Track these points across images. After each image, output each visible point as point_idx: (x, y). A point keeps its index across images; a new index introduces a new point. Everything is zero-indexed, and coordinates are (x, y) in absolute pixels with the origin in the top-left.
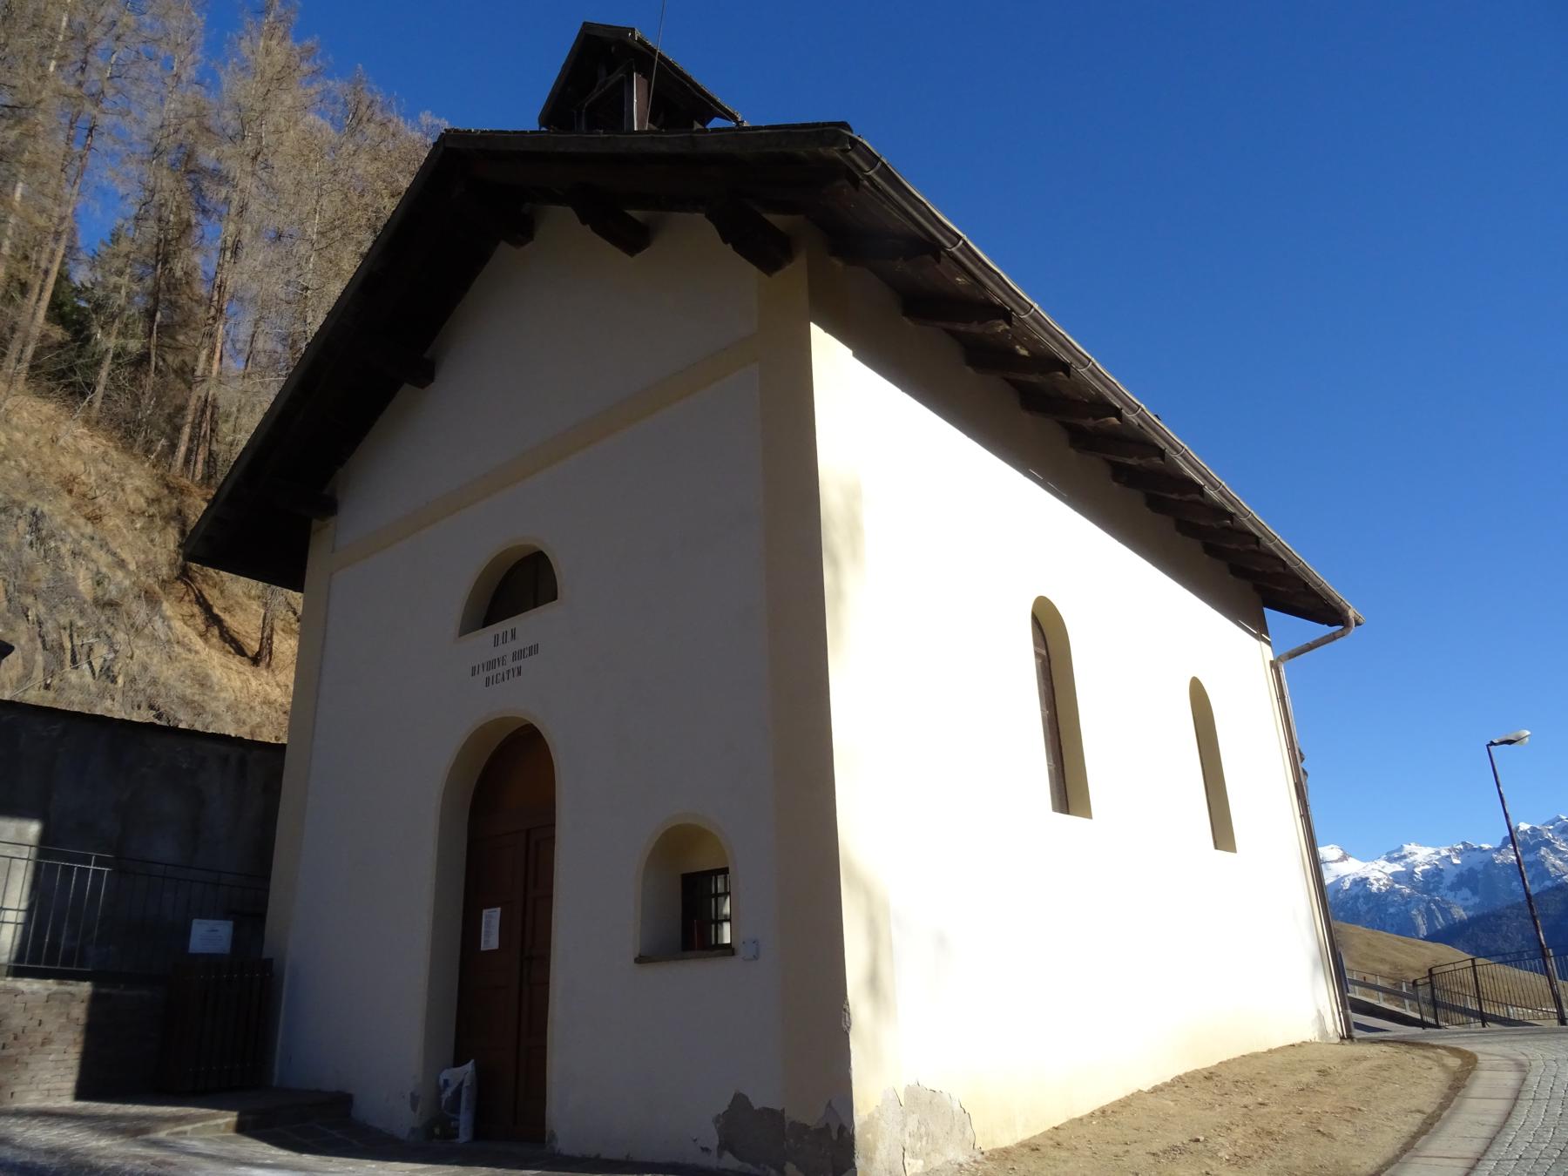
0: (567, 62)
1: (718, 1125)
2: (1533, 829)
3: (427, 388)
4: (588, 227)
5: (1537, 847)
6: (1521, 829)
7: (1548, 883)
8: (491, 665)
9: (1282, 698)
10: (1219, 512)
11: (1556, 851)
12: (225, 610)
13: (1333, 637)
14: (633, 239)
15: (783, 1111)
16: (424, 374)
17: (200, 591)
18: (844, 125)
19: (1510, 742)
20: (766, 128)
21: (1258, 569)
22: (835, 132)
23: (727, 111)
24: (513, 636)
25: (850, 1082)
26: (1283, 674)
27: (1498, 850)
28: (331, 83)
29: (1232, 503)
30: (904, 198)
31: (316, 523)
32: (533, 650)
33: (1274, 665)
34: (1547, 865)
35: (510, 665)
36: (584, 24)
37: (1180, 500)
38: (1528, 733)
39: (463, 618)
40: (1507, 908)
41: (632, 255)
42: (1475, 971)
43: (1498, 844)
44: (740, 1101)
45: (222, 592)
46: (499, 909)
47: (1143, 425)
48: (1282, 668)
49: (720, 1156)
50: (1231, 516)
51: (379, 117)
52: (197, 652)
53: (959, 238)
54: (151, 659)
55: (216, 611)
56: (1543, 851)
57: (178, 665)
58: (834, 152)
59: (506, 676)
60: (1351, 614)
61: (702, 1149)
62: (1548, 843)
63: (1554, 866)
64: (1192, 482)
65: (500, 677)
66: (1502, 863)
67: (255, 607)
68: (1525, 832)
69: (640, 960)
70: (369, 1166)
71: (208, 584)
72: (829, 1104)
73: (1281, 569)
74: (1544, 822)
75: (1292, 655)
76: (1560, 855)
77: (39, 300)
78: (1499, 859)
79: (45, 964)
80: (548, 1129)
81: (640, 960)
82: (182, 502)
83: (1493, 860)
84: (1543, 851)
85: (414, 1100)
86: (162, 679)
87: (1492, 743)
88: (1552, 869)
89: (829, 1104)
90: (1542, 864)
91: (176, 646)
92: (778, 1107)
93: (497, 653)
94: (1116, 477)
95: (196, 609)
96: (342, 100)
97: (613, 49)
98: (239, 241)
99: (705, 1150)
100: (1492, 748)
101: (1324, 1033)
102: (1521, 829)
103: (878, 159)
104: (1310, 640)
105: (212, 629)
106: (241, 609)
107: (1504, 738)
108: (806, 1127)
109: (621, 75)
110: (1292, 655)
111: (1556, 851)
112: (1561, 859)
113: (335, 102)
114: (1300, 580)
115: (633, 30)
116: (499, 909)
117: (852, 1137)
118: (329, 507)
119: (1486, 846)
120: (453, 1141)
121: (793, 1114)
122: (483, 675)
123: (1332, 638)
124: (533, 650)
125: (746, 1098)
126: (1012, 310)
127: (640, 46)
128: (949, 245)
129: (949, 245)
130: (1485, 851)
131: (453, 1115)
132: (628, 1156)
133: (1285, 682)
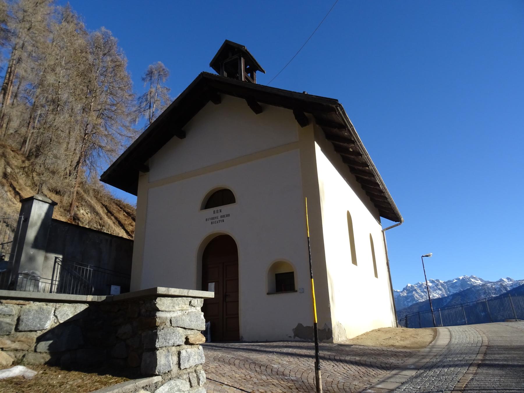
0: (220, 50)
2: (412, 286)
3: (183, 139)
4: (249, 106)
5: (412, 291)
6: (408, 286)
7: (414, 302)
8: (213, 219)
9: (384, 240)
10: (381, 191)
11: (417, 293)
12: (20, 189)
13: (397, 225)
14: (258, 110)
16: (182, 135)
17: (11, 183)
18: (337, 100)
19: (427, 256)
20: (314, 96)
21: (384, 206)
22: (335, 101)
23: (262, 70)
24: (221, 211)
25: (331, 319)
26: (385, 234)
27: (402, 292)
28: (58, 7)
29: (385, 190)
30: (345, 117)
31: (141, 173)
32: (228, 215)
33: (383, 232)
34: (415, 297)
35: (220, 219)
36: (226, 40)
37: (373, 188)
38: (432, 254)
39: (202, 205)
40: (403, 309)
41: (257, 114)
42: (419, 315)
43: (402, 290)
44: (300, 326)
45: (17, 182)
46: (214, 283)
47: (373, 170)
48: (384, 232)
49: (294, 338)
50: (383, 193)
51: (75, 22)
52: (16, 204)
53: (352, 126)
54: (3, 205)
55: (17, 190)
56: (414, 292)
57: (12, 208)
58: (334, 106)
59: (218, 222)
60: (402, 219)
61: (289, 337)
62: (415, 290)
63: (416, 297)
64: (378, 184)
65: (216, 222)
66: (403, 296)
67: (29, 189)
68: (409, 287)
69: (268, 294)
71: (13, 180)
73: (390, 207)
74: (415, 284)
75: (387, 229)
76: (418, 294)
78: (402, 294)
80: (240, 336)
81: (268, 294)
82: (5, 150)
83: (400, 295)
84: (414, 292)
86: (8, 213)
87: (423, 256)
88: (416, 298)
89: (325, 324)
90: (413, 296)
91: (9, 201)
93: (216, 215)
94: (357, 180)
95: (11, 189)
96: (61, 13)
97: (236, 50)
98: (20, 58)
99: (290, 337)
100: (423, 257)
101: (393, 326)
102: (408, 286)
103: (343, 109)
104: (392, 225)
105: (17, 196)
106: (25, 190)
107: (426, 255)
109: (237, 57)
110: (387, 229)
111: (417, 293)
112: (418, 295)
113: (59, 14)
114: (393, 210)
115: (244, 47)
116: (214, 283)
117: (332, 331)
118: (146, 169)
119: (398, 291)
122: (210, 221)
123: (397, 225)
124: (228, 215)
126: (356, 141)
127: (246, 52)
128: (349, 127)
129: (349, 127)
130: (398, 292)
133: (385, 236)
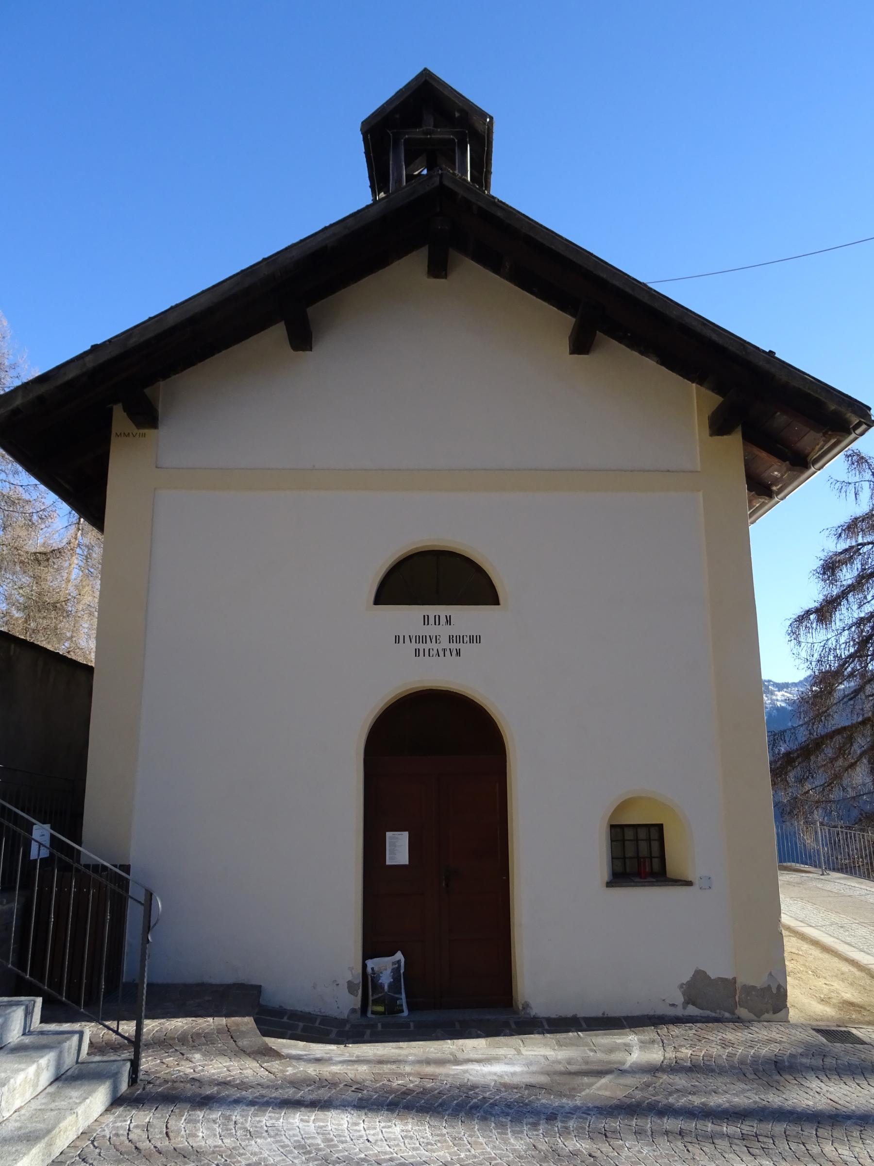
1: (683, 990)
15: (734, 979)
32: (475, 639)
49: (684, 1008)
70: (517, 1069)
72: (770, 974)
77: (855, 841)
79: (401, 993)
85: (351, 987)
89: (770, 974)
92: (729, 976)
99: (673, 1005)
108: (754, 988)
120: (400, 1015)
121: (743, 980)
124: (475, 639)
125: (704, 973)
131: (397, 996)
132: (603, 1014)
